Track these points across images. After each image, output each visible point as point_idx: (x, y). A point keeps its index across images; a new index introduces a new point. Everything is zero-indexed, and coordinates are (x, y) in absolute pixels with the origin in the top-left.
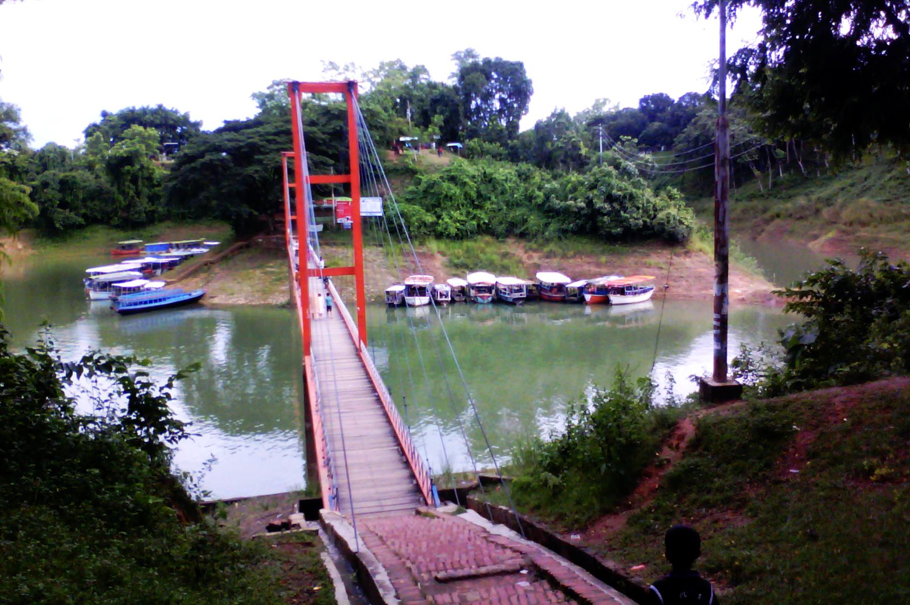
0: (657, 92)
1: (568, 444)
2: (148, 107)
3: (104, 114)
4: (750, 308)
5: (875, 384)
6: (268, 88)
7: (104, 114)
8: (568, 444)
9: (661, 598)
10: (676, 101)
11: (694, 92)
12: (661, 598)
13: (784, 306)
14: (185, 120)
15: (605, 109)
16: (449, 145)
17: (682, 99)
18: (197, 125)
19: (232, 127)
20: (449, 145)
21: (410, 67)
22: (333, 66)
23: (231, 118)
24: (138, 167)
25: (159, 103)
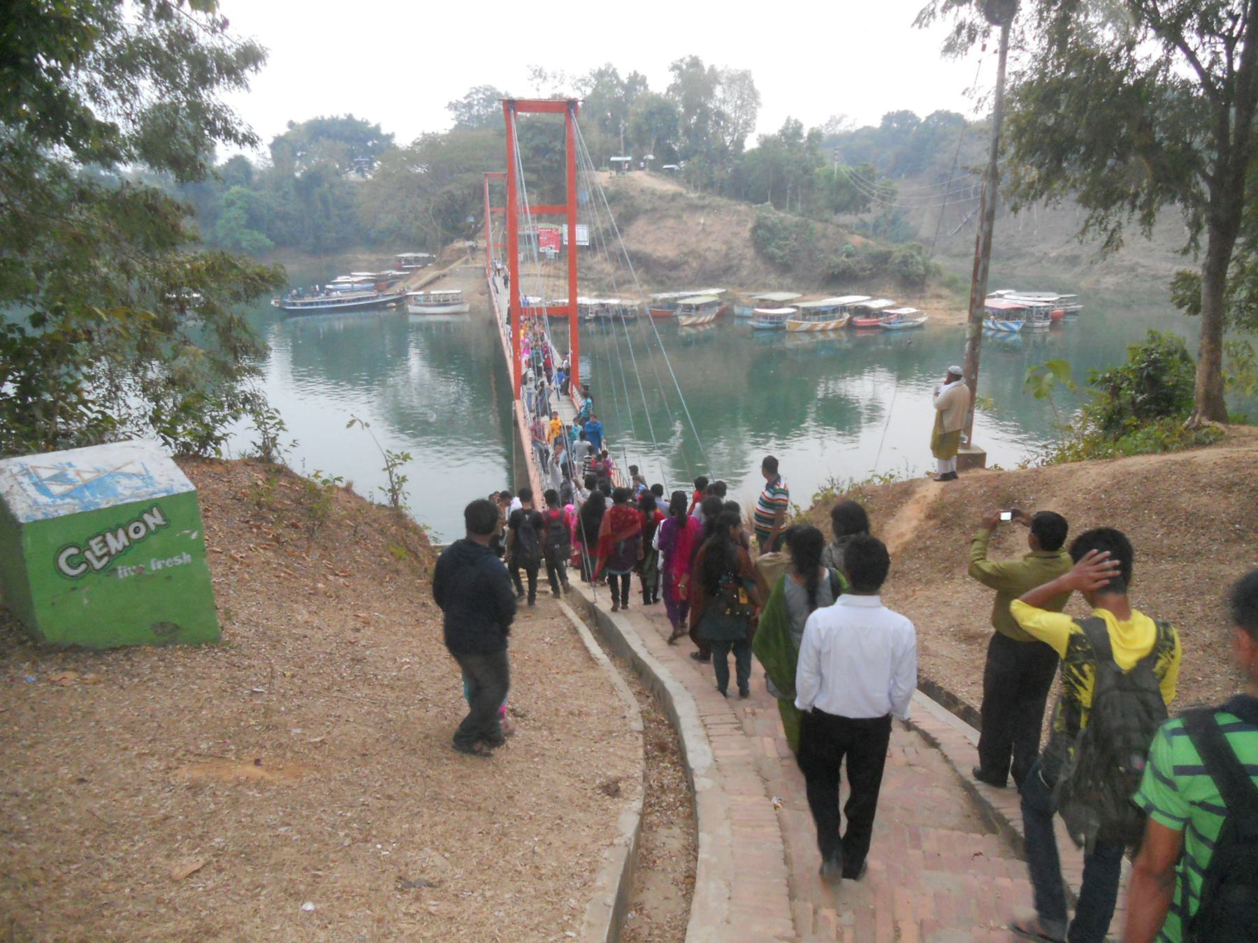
0: (902, 109)
1: (1106, 208)
2: (322, 117)
3: (291, 124)
4: (773, 593)
5: (1203, 297)
6: (465, 98)
7: (291, 124)
8: (1106, 208)
9: (844, 761)
10: (923, 120)
11: (946, 109)
12: (844, 761)
13: (1139, 229)
14: (375, 133)
15: (841, 128)
16: (665, 167)
17: (928, 118)
18: (390, 137)
19: (430, 144)
20: (665, 167)
21: (624, 77)
22: (539, 74)
23: (428, 131)
24: (327, 185)
25: (682, 53)
